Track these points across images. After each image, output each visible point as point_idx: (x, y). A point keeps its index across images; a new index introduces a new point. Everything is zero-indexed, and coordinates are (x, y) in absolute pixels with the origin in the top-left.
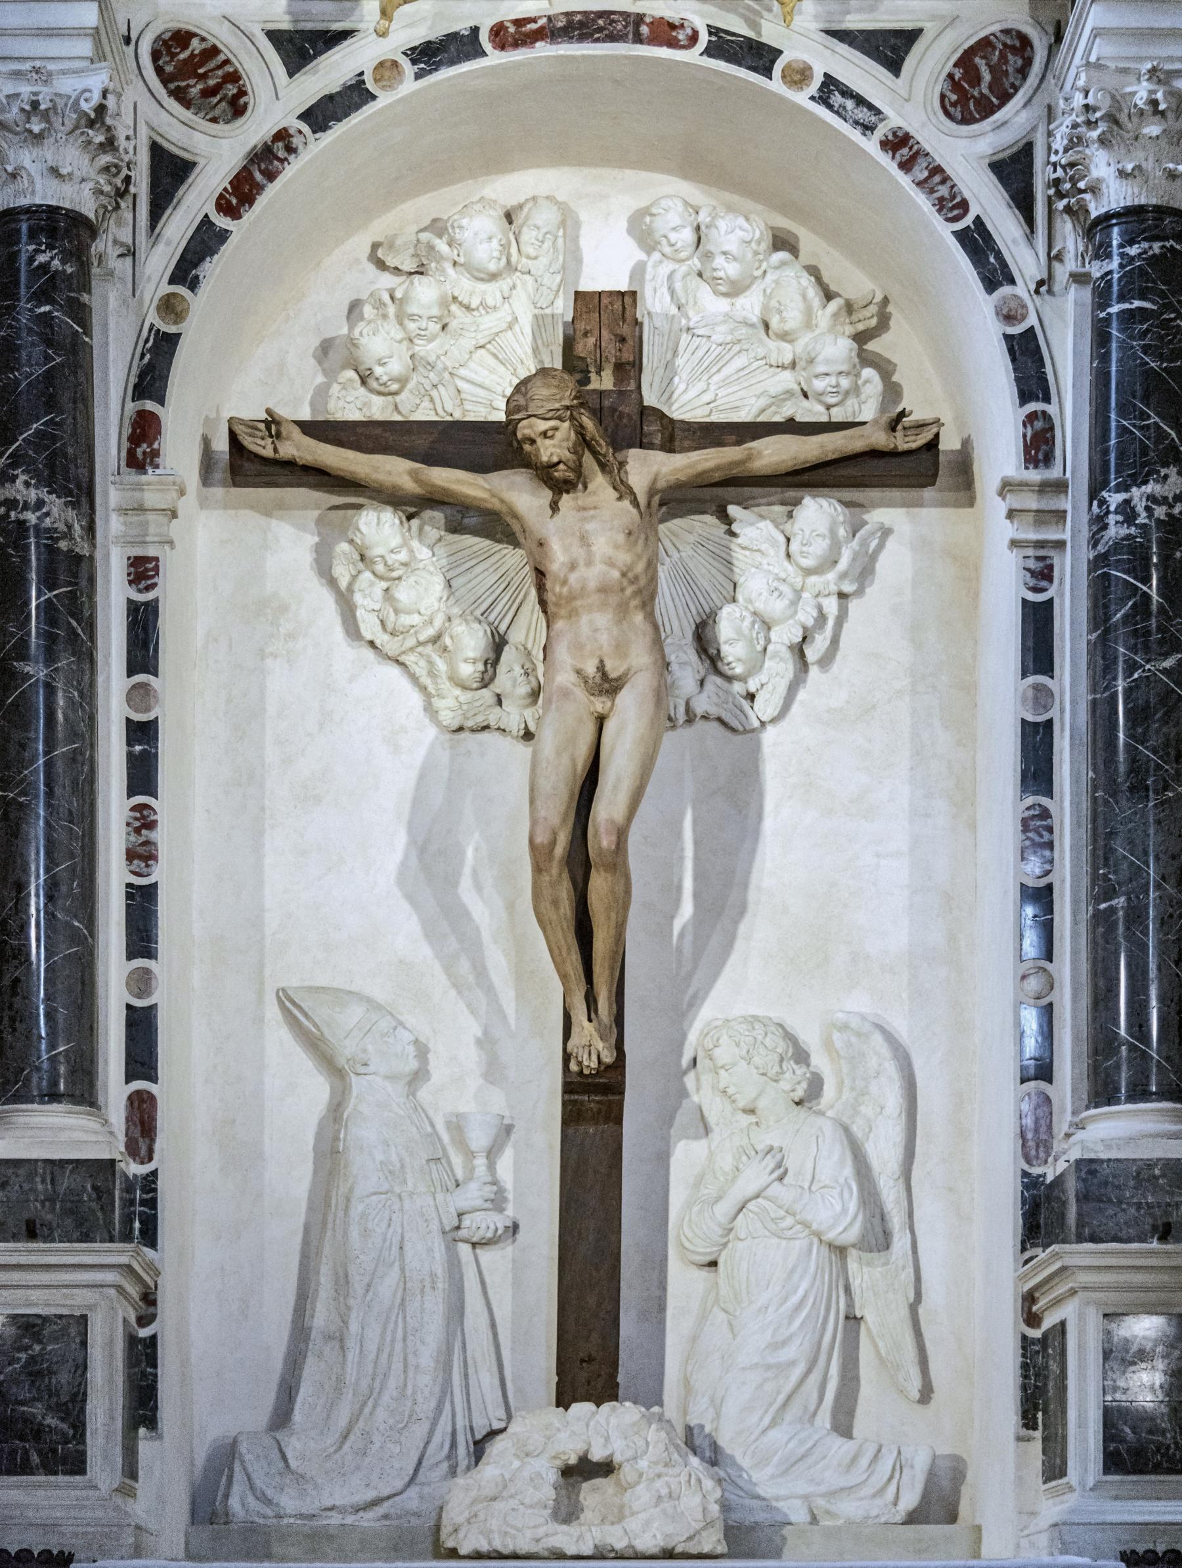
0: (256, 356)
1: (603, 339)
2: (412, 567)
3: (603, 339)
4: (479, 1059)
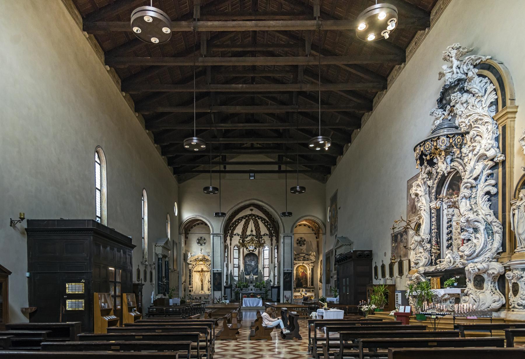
0: (195, 269)
1: (202, 269)
2: (198, 273)
3: (202, 269)
4: (200, 283)
